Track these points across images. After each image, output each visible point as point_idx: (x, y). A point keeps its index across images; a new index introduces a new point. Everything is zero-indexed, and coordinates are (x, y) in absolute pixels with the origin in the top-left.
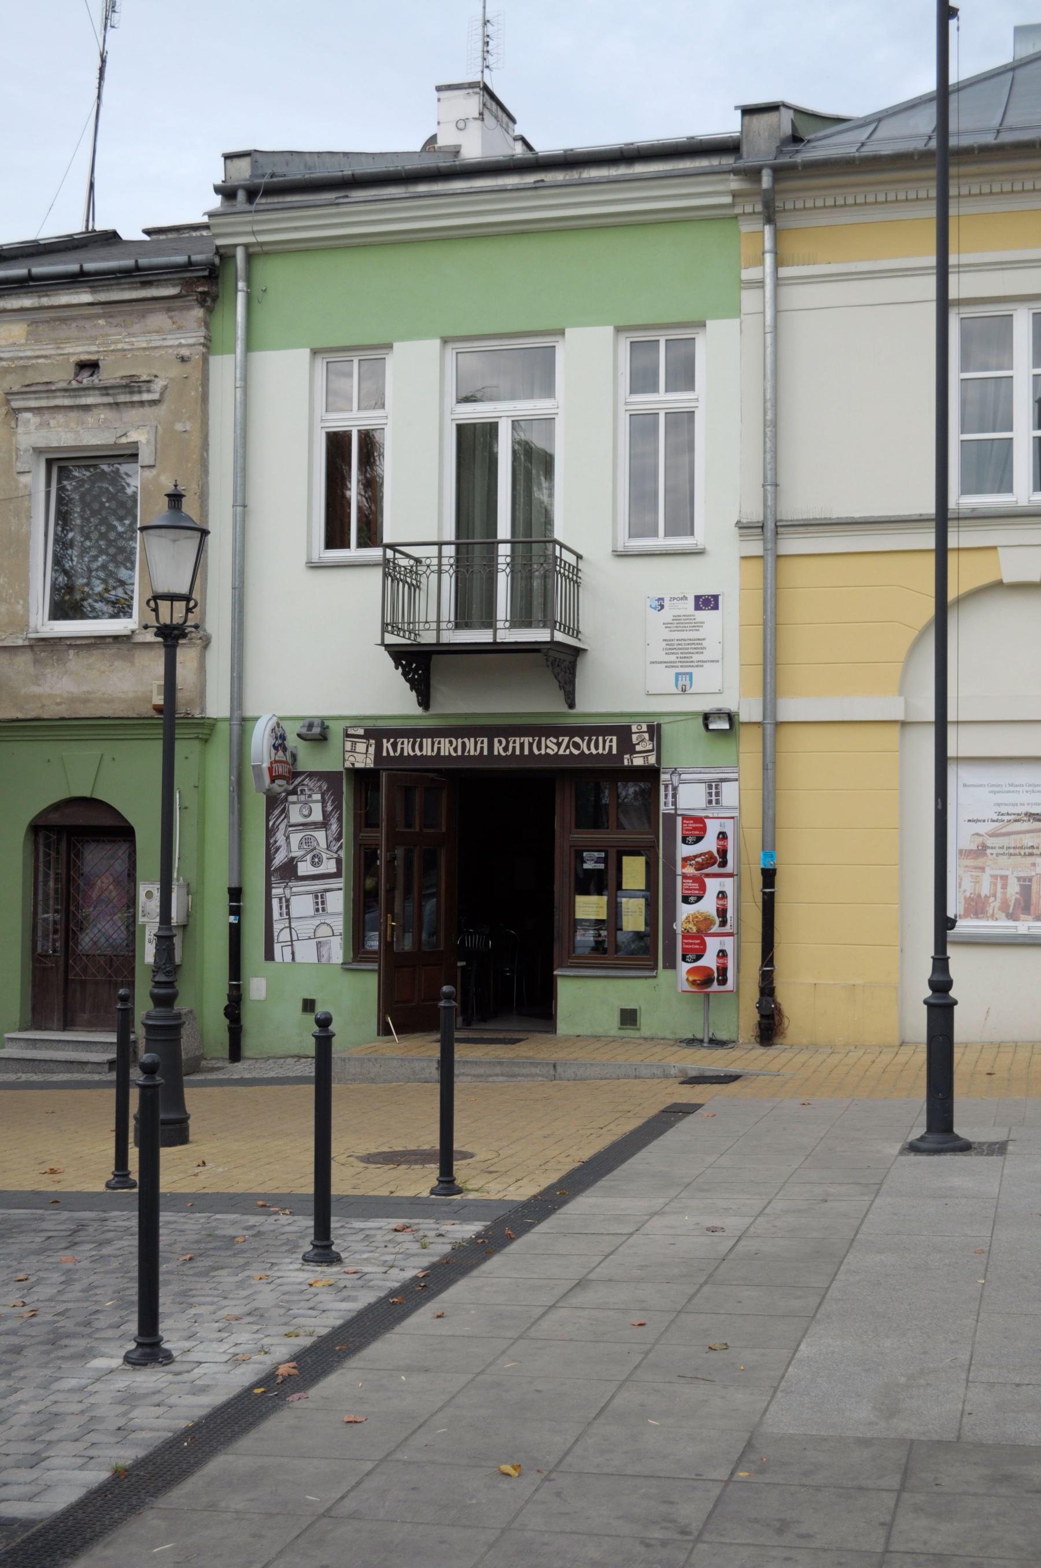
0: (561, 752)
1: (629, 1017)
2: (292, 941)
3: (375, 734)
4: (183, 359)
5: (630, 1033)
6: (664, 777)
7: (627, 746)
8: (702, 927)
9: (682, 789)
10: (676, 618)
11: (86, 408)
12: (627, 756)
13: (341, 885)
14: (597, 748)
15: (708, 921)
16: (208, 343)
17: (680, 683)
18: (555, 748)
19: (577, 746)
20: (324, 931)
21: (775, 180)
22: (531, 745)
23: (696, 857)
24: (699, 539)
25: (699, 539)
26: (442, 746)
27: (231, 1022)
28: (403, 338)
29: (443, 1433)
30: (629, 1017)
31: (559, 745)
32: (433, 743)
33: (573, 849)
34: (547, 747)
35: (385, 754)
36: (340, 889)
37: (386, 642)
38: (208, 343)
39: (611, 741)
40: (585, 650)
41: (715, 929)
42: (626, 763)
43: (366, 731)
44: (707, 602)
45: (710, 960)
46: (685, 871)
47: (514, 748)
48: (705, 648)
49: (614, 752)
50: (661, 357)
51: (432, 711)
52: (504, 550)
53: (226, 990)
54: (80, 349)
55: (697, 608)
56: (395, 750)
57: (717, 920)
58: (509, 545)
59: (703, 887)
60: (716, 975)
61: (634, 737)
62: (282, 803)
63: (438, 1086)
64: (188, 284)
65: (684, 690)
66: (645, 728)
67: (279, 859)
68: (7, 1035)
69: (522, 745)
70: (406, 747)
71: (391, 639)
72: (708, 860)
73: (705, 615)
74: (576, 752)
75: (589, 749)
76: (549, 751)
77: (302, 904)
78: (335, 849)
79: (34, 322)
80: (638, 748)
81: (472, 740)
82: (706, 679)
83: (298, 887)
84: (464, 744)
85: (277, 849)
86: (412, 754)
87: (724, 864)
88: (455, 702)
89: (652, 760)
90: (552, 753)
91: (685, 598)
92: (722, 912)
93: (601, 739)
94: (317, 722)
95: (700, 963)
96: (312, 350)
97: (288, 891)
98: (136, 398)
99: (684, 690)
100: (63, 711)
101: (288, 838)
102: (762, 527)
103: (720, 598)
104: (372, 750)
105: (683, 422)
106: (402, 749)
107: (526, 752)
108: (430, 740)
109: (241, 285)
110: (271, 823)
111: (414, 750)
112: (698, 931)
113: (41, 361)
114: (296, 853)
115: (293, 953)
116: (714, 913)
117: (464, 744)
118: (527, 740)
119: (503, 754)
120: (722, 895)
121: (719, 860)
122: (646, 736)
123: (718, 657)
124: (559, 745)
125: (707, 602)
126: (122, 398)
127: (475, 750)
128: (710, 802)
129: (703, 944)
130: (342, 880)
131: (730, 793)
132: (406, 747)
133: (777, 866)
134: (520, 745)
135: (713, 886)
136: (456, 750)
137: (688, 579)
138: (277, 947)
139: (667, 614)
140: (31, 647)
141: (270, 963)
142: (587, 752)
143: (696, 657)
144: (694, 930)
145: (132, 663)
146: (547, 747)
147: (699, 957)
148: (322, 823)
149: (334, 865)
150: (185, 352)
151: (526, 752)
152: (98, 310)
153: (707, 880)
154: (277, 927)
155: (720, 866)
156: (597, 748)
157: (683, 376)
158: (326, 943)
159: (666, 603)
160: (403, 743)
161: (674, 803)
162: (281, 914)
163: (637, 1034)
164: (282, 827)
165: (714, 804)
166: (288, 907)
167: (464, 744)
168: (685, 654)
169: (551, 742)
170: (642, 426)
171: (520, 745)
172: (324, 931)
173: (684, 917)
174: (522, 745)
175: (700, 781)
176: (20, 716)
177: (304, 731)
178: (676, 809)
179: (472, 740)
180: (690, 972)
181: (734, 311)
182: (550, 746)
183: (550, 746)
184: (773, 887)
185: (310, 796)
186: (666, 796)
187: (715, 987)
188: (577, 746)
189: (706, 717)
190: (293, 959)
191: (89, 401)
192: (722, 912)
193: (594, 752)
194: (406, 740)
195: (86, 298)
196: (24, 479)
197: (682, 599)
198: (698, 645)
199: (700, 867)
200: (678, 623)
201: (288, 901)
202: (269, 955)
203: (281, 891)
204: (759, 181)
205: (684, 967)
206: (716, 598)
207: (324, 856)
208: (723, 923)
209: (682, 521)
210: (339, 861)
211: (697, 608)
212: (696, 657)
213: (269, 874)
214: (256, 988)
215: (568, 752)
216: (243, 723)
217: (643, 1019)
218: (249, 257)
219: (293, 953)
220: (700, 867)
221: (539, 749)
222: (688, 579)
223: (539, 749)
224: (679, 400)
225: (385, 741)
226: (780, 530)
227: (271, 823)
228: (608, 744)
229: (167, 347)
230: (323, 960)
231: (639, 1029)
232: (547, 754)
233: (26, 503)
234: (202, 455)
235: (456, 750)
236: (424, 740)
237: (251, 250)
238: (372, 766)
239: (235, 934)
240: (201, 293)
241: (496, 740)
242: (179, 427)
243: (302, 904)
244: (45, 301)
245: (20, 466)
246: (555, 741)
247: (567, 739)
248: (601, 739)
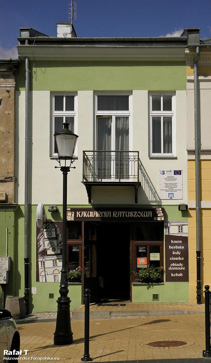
0: (134, 216)
1: (155, 297)
2: (45, 275)
4: (8, 91)
7: (155, 215)
9: (171, 228)
10: (168, 177)
14: (146, 215)
18: (133, 215)
19: (139, 214)
20: (56, 272)
21: (200, 51)
22: (125, 214)
24: (174, 154)
25: (174, 154)
26: (84, 214)
28: (81, 90)
30: (155, 297)
31: (134, 214)
32: (148, 213)
33: (136, 246)
34: (130, 215)
35: (77, 216)
36: (61, 259)
39: (150, 213)
44: (178, 173)
47: (119, 215)
49: (151, 216)
50: (161, 100)
52: (113, 154)
55: (175, 174)
56: (81, 215)
58: (130, 150)
62: (42, 231)
63: (70, 310)
64: (10, 69)
65: (171, 198)
67: (41, 249)
69: (122, 214)
70: (84, 214)
74: (139, 216)
75: (143, 215)
76: (130, 216)
77: (49, 263)
78: (60, 246)
80: (158, 215)
81: (106, 212)
82: (177, 195)
83: (47, 258)
84: (103, 214)
85: (40, 246)
86: (86, 216)
89: (163, 219)
90: (132, 216)
93: (147, 212)
94: (54, 206)
97: (44, 259)
99: (171, 198)
101: (44, 242)
102: (195, 151)
104: (73, 215)
105: (168, 121)
106: (83, 215)
107: (123, 216)
108: (92, 212)
110: (38, 238)
111: (87, 215)
114: (46, 247)
115: (46, 279)
117: (103, 214)
118: (123, 212)
119: (116, 217)
122: (161, 211)
123: (182, 189)
124: (134, 214)
125: (178, 173)
127: (107, 215)
128: (179, 231)
131: (185, 229)
132: (84, 214)
134: (121, 214)
136: (101, 215)
137: (173, 165)
138: (40, 277)
141: (38, 283)
142: (143, 216)
143: (174, 189)
146: (130, 215)
148: (55, 238)
149: (60, 251)
151: (123, 216)
154: (40, 271)
156: (146, 215)
157: (168, 106)
158: (57, 275)
160: (83, 213)
161: (169, 232)
162: (42, 267)
163: (158, 302)
164: (42, 239)
166: (44, 264)
167: (103, 213)
168: (171, 189)
169: (131, 213)
170: (156, 122)
171: (121, 214)
172: (56, 272)
174: (122, 214)
177: (51, 209)
178: (169, 234)
179: (106, 212)
181: (184, 88)
182: (131, 214)
183: (131, 214)
185: (51, 229)
188: (139, 214)
189: (180, 206)
190: (46, 281)
193: (145, 216)
194: (84, 212)
198: (175, 185)
200: (169, 178)
201: (44, 262)
202: (38, 280)
203: (42, 259)
204: (195, 51)
206: (180, 171)
207: (56, 248)
209: (168, 148)
210: (61, 250)
211: (175, 174)
212: (174, 189)
213: (37, 254)
214: (34, 290)
215: (136, 216)
216: (29, 206)
217: (160, 297)
218: (30, 62)
219: (46, 279)
221: (127, 215)
222: (173, 165)
223: (127, 215)
224: (167, 113)
225: (77, 212)
227: (38, 238)
229: (2, 87)
230: (56, 281)
231: (159, 300)
232: (130, 217)
235: (101, 215)
236: (90, 212)
238: (73, 220)
240: (14, 71)
241: (114, 212)
242: (6, 112)
243: (49, 263)
246: (133, 213)
247: (136, 212)
248: (147, 212)
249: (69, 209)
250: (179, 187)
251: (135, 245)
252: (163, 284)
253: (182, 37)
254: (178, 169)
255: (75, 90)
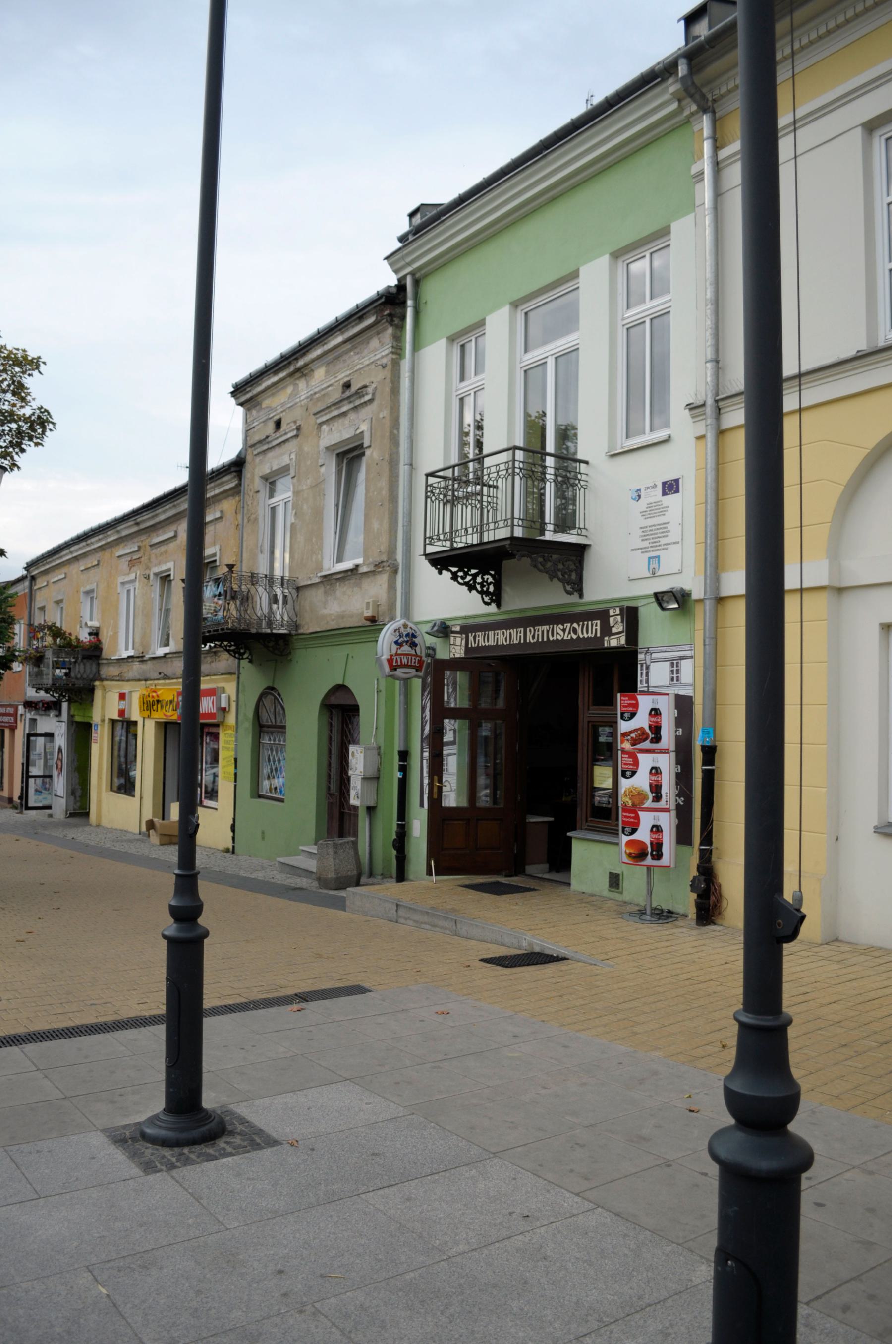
0: (565, 638)
3: (467, 629)
5: (615, 895)
6: (641, 656)
8: (637, 802)
9: (653, 666)
11: (344, 414)
12: (606, 638)
13: (455, 751)
14: (587, 633)
15: (640, 796)
16: (399, 351)
17: (652, 567)
18: (561, 633)
23: (631, 732)
27: (398, 852)
28: (491, 311)
29: (101, 1292)
31: (564, 630)
34: (557, 633)
37: (427, 552)
38: (399, 351)
40: (589, 545)
41: (649, 804)
42: (606, 645)
43: (461, 627)
44: (671, 487)
45: (643, 835)
46: (623, 746)
48: (668, 531)
49: (598, 635)
51: (503, 609)
53: (395, 828)
54: (343, 375)
55: (664, 494)
57: (651, 796)
59: (636, 763)
60: (649, 849)
61: (611, 619)
65: (654, 573)
66: (618, 612)
68: (301, 848)
71: (430, 549)
72: (640, 736)
73: (671, 499)
74: (575, 637)
79: (328, 364)
80: (614, 630)
82: (670, 560)
87: (657, 739)
88: (521, 599)
90: (560, 638)
91: (655, 486)
92: (656, 789)
95: (635, 837)
96: (448, 338)
98: (362, 401)
99: (654, 573)
100: (333, 625)
103: (680, 481)
104: (464, 642)
107: (545, 639)
109: (410, 302)
112: (633, 804)
113: (330, 389)
116: (646, 788)
118: (545, 628)
120: (655, 771)
121: (651, 736)
122: (619, 618)
124: (564, 630)
125: (671, 487)
126: (357, 402)
128: (672, 679)
129: (637, 818)
130: (455, 747)
133: (717, 743)
135: (646, 762)
139: (643, 504)
140: (321, 582)
142: (581, 636)
144: (630, 804)
145: (361, 588)
147: (634, 831)
150: (384, 361)
152: (348, 346)
153: (641, 756)
155: (652, 742)
159: (643, 494)
161: (647, 682)
165: (675, 682)
168: (654, 538)
169: (558, 629)
173: (623, 791)
175: (665, 660)
176: (318, 630)
178: (648, 687)
180: (630, 843)
182: (560, 633)
184: (713, 764)
186: (642, 674)
187: (649, 861)
191: (344, 409)
192: (656, 789)
193: (586, 636)
195: (340, 339)
196: (323, 470)
197: (653, 487)
198: (663, 529)
199: (634, 743)
205: (625, 839)
208: (658, 798)
211: (664, 494)
212: (663, 541)
220: (634, 743)
221: (553, 636)
223: (553, 636)
226: (721, 404)
228: (594, 628)
231: (622, 893)
233: (571, 507)
234: (391, 433)
237: (418, 275)
239: (403, 784)
244: (327, 347)
245: (321, 462)
246: (562, 627)
249: (458, 629)
250: (674, 534)
251: (589, 722)
252: (429, 873)
253: (712, 31)
254: (669, 477)
255: (576, 268)
